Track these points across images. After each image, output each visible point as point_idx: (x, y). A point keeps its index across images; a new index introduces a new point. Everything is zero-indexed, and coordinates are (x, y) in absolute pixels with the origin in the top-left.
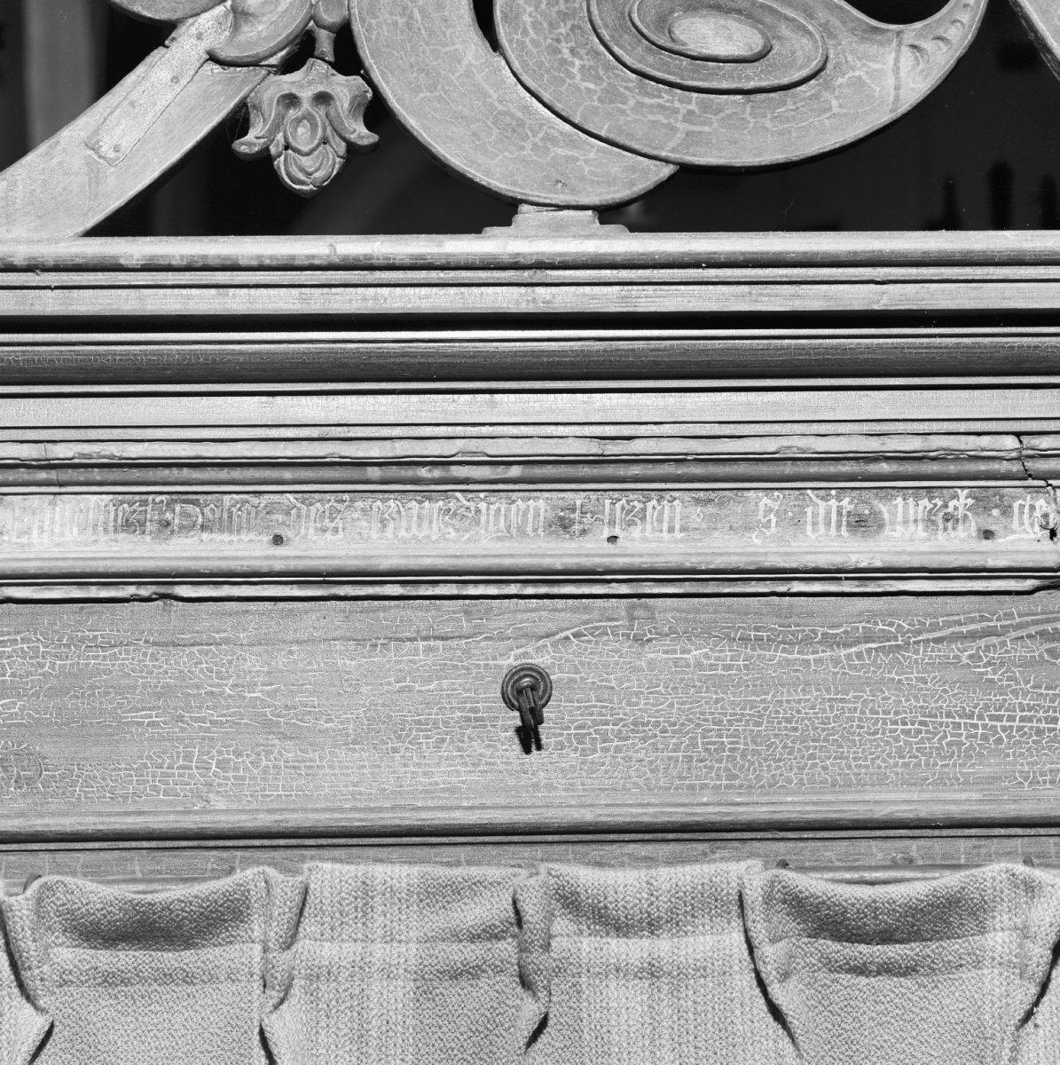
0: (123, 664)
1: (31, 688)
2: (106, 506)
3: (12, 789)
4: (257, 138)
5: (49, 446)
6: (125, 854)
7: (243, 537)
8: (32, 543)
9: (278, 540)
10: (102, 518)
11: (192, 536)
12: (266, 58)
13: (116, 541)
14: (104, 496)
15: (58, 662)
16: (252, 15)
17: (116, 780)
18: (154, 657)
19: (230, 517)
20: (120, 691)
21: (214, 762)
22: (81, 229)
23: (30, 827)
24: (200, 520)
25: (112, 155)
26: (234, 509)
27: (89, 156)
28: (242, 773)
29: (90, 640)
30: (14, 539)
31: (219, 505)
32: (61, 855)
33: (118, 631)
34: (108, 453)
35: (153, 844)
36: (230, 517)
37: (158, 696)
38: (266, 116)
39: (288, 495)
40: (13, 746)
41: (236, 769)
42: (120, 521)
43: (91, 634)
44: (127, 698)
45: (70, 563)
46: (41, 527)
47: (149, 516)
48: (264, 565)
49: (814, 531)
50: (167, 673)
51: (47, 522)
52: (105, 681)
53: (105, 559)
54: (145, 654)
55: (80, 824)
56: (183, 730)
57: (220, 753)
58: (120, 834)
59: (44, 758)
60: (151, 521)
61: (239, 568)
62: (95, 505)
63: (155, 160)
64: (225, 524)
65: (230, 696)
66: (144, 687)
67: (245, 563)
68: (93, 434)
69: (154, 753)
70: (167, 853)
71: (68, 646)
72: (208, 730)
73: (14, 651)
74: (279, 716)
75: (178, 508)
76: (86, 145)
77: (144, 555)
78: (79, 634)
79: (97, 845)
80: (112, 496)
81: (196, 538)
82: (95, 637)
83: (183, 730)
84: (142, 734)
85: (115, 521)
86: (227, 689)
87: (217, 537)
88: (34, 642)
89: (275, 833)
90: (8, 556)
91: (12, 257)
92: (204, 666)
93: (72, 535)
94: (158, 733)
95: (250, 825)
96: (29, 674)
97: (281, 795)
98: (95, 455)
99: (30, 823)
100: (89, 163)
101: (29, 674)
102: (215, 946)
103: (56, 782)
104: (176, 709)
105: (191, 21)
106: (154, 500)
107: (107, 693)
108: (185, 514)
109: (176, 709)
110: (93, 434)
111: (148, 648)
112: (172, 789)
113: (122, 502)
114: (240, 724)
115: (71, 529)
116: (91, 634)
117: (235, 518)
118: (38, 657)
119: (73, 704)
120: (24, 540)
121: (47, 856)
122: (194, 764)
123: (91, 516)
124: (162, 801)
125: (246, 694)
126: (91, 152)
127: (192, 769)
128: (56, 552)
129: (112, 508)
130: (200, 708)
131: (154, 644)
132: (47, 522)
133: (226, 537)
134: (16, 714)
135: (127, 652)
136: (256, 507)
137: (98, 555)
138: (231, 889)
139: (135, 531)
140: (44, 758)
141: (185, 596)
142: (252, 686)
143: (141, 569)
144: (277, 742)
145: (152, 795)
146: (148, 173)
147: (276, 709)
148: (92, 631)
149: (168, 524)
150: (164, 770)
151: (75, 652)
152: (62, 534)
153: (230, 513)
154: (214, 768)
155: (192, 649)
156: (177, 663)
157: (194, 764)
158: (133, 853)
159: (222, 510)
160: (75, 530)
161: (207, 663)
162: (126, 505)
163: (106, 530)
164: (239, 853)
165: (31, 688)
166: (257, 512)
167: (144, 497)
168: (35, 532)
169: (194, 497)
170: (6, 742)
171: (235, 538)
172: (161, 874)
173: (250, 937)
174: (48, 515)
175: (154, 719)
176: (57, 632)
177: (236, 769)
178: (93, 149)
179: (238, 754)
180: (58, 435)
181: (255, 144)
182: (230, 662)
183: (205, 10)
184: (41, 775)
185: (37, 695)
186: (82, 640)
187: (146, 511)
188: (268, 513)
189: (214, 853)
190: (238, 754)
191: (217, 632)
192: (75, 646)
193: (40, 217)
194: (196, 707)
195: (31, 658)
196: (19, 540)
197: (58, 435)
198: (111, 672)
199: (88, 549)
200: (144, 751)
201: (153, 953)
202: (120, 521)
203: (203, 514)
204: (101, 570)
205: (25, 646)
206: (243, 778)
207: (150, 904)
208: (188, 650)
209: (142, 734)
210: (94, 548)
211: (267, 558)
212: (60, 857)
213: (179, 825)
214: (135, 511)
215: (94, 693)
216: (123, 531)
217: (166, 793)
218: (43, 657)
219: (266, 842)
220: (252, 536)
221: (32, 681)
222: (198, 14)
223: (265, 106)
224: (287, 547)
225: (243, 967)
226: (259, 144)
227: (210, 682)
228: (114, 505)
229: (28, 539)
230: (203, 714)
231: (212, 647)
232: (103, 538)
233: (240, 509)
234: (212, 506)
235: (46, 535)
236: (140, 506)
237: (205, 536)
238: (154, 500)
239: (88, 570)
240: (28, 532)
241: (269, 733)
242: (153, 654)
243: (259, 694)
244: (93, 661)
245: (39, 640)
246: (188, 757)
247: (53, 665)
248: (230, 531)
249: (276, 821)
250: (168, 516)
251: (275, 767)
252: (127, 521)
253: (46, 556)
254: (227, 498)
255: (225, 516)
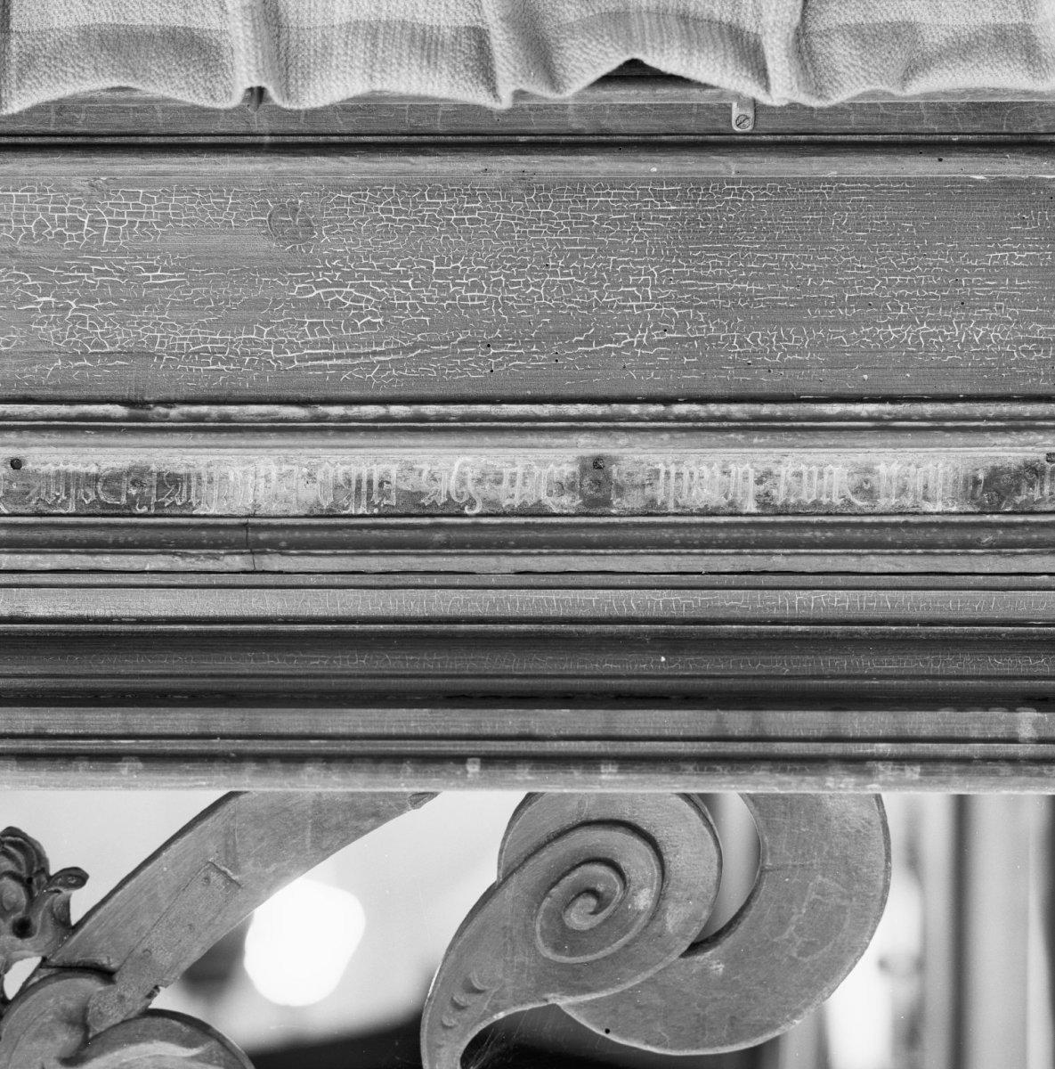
0: (185, 333)
1: (282, 310)
2: (200, 503)
3: (300, 201)
4: (59, 892)
5: (250, 568)
6: (173, 130)
7: (53, 468)
8: (276, 464)
9: (16, 464)
10: (204, 490)
11: (107, 469)
12: (50, 976)
13: (188, 466)
14: (202, 513)
15: (253, 337)
16: (63, 1021)
17: (190, 209)
18: (153, 340)
19: (67, 489)
20: (187, 306)
21: (86, 227)
22: (242, 797)
23: (268, 161)
24: (99, 487)
25: (214, 876)
26: (64, 497)
27: (236, 873)
28: (56, 215)
29: (220, 359)
30: (296, 468)
31: (79, 502)
32: (242, 129)
33: (191, 370)
34: (188, 560)
35: (141, 140)
36: (67, 489)
37: (147, 300)
38: (49, 915)
39: (6, 512)
40: (300, 248)
41: (62, 220)
42: (185, 487)
43: (220, 366)
44: (180, 298)
45: (232, 443)
46: (268, 481)
47: (154, 492)
48: (27, 437)
49: (746, 473)
50: (138, 324)
51: (262, 486)
52: (203, 317)
53: (196, 447)
54: (162, 344)
55: (216, 163)
56: (120, 263)
57: (80, 238)
58: (173, 152)
59: (266, 234)
60: (151, 486)
61: (54, 435)
62: (211, 506)
63: (165, 869)
64: (70, 481)
65: (71, 298)
66: (162, 308)
67: (46, 440)
68: (205, 579)
69: (150, 238)
70: (128, 130)
71: (245, 354)
72: (94, 262)
73: (301, 350)
74: (19, 277)
75: (124, 500)
76: (239, 886)
77: (156, 450)
78: (232, 367)
79: (201, 140)
80: (194, 512)
81: (104, 467)
82: (214, 363)
83: (120, 263)
84: (163, 258)
85: (189, 488)
86: (74, 306)
87: (81, 469)
88: (279, 359)
89: (9, 150)
90: (300, 451)
91: (256, 771)
92: (99, 331)
93: (235, 473)
94: (146, 260)
95: (35, 160)
96: (284, 325)
97: (13, 191)
98: (202, 558)
99: (269, 165)
100: (236, 867)
101: (284, 325)
102: (58, 30)
103: (254, 209)
104: (128, 286)
105: (132, 1016)
106: (149, 509)
107: (200, 302)
108: (117, 493)
109: (128, 286)
110: (205, 579)
111: (159, 351)
112: (130, 199)
113: (183, 506)
114: (59, 268)
115: (235, 479)
116: (220, 366)
117: (62, 489)
118: (276, 343)
119: (238, 292)
120: (285, 468)
121: (255, 129)
122: (107, 225)
123: (216, 492)
124: (140, 187)
125: (53, 300)
126: (234, 878)
127: (110, 221)
128: (253, 454)
129: (194, 501)
130: (102, 286)
131: (152, 355)
132: (262, 486)
133: (71, 468)
134: (297, 283)
135: (181, 347)
136: (40, 499)
137: (205, 450)
138: (34, 90)
139: (168, 476)
140: (266, 234)
141: (118, 406)
142: (47, 307)
143: (158, 435)
144: (20, 248)
145: (151, 193)
146: (173, 856)
147: (21, 284)
148: (218, 370)
149: (133, 483)
150: (139, 220)
151: (236, 347)
152: (245, 473)
153: (67, 494)
154: (86, 221)
155: (112, 349)
156: (128, 334)
157: (107, 225)
158: (165, 131)
159: (76, 497)
160: (232, 478)
161: (96, 333)
162: (179, 503)
163: (199, 477)
164: (52, 129)
165: (282, 310)
166: (39, 494)
167: (160, 512)
168: (274, 476)
169: (106, 512)
170: (308, 252)
171: (62, 467)
172: (134, 108)
173: (21, 37)
174: (260, 494)
175: (150, 274)
176: (256, 369)
177: (62, 220)
178: (232, 881)
179: (61, 236)
180: (241, 580)
181: (61, 885)
182: (71, 334)
183: (115, 1026)
184: (270, 216)
185: (276, 302)
186: (229, 360)
187: (158, 497)
188: (27, 493)
189: (77, 130)
190: (61, 236)
191: (85, 366)
192: (236, 354)
193: (286, 809)
194: (106, 287)
195: (282, 342)
196: (290, 467)
197: (241, 580)
198: (198, 325)
199: (217, 458)
200: (161, 240)
201: (123, 22)
202: (185, 487)
203: (96, 493)
204: (200, 436)
205: (290, 355)
206: (54, 210)
207: (116, 76)
208: (116, 348)
209: (163, 258)
210: (211, 458)
211: (24, 446)
212: (242, 128)
213: (111, 160)
214: (168, 497)
215: (215, 303)
216: (181, 476)
217: (136, 195)
218: (270, 343)
219: (21, 140)
220: (44, 469)
221: (281, 317)
222: (123, 1022)
223: (49, 923)
224: (6, 456)
225: (28, 6)
226: (56, 885)
227: (91, 313)
228: (191, 504)
229: (280, 469)
230: (99, 279)
231: (91, 351)
232: (202, 469)
233: (58, 497)
234: (87, 502)
235: (262, 473)
236: (164, 503)
237: (93, 470)
238: (149, 509)
239: (214, 435)
240: (282, 476)
241: (27, 258)
242: (154, 345)
243: (39, 300)
244: (218, 337)
245: (275, 361)
246: (114, 234)
247: (260, 333)
248: (67, 475)
249: (7, 163)
250: (133, 492)
251: (21, 222)
252: (177, 487)
253: (260, 450)
254: (72, 509)
255: (73, 491)
